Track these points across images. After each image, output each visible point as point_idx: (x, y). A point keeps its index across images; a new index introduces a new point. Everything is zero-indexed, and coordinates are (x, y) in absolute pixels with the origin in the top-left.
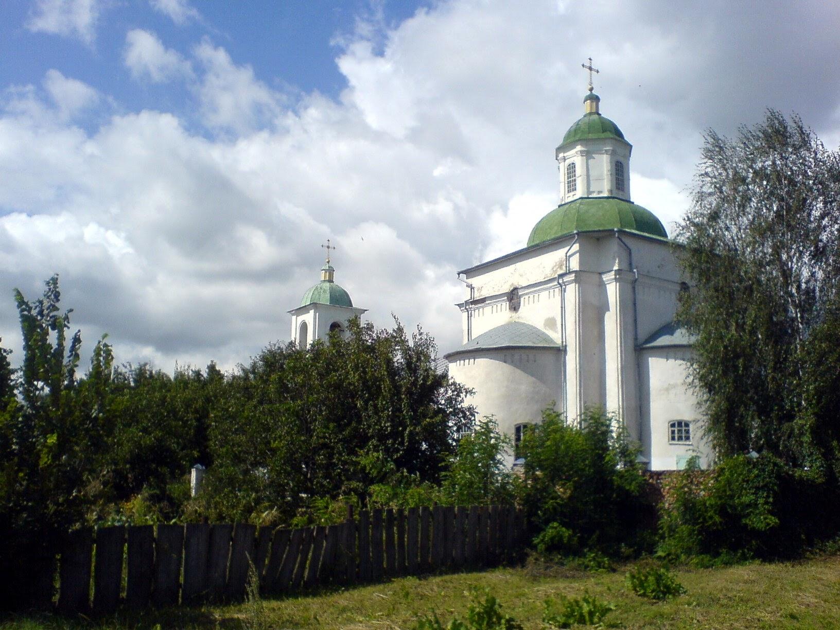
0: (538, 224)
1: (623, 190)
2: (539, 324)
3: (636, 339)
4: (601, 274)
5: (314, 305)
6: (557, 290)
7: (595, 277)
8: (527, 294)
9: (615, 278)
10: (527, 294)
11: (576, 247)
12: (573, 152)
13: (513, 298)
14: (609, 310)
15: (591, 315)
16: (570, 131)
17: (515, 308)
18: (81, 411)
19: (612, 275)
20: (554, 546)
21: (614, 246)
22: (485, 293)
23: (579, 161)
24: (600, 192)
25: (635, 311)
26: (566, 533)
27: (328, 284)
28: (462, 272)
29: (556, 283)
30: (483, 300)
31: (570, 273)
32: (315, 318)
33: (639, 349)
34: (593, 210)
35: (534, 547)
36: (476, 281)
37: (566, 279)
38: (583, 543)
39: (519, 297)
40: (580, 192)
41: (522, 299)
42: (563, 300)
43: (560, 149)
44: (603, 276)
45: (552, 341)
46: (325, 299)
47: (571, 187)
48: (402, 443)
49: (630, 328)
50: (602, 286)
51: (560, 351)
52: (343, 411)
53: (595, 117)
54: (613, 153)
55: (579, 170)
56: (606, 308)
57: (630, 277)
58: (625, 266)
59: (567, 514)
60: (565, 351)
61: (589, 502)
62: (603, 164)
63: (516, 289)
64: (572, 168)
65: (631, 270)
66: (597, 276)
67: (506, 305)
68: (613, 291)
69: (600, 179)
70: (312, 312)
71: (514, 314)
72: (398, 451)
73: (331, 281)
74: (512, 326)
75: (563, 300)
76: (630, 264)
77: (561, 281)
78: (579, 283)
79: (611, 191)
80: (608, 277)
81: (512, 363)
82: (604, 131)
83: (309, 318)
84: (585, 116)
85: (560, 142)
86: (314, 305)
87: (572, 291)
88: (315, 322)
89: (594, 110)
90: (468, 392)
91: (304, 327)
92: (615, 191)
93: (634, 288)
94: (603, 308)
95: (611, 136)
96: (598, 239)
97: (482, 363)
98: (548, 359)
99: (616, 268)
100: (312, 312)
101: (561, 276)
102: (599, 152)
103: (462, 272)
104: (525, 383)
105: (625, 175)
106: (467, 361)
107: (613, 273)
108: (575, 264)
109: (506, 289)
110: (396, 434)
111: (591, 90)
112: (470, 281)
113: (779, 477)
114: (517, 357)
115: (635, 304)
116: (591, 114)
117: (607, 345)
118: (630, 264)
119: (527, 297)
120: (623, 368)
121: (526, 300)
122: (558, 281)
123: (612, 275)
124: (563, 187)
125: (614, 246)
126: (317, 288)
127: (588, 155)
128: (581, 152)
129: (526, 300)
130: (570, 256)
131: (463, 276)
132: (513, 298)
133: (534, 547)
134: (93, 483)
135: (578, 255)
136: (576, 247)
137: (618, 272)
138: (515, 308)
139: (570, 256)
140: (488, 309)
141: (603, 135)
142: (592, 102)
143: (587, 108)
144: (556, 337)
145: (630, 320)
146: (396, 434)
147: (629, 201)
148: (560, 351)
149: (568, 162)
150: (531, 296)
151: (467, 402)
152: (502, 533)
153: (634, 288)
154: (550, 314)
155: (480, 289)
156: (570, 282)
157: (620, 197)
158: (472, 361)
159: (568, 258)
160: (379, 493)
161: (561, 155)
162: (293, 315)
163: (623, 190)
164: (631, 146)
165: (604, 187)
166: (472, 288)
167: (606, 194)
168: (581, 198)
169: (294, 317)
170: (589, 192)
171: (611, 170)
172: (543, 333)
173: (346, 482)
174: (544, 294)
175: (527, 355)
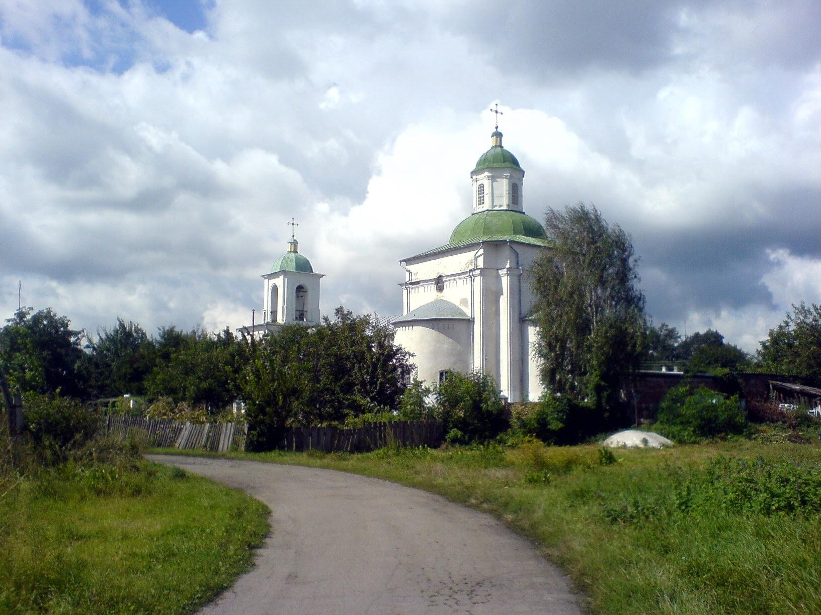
0: (458, 226)
2: (457, 303)
5: (284, 272)
7: (494, 272)
11: (481, 251)
12: (482, 176)
13: (439, 283)
15: (491, 297)
17: (440, 289)
19: (505, 271)
20: (455, 441)
21: (506, 251)
22: (420, 277)
23: (487, 183)
24: (501, 206)
26: (460, 433)
27: (293, 255)
28: (404, 261)
30: (418, 283)
34: (495, 221)
35: (445, 440)
36: (412, 268)
38: (470, 439)
39: (443, 282)
40: (487, 206)
42: (472, 286)
45: (465, 314)
46: (292, 267)
47: (481, 201)
48: (375, 388)
49: (517, 307)
50: (498, 278)
51: (470, 322)
52: (340, 369)
53: (499, 149)
55: (487, 190)
57: (516, 272)
58: (514, 265)
59: (462, 424)
61: (474, 417)
62: (503, 185)
63: (441, 276)
64: (481, 188)
65: (518, 268)
67: (434, 287)
68: (505, 281)
69: (501, 196)
70: (282, 277)
72: (372, 392)
73: (295, 252)
74: (439, 304)
75: (472, 286)
76: (518, 263)
79: (508, 206)
80: (502, 272)
81: (438, 330)
83: (279, 281)
85: (473, 167)
86: (284, 272)
87: (478, 281)
91: (275, 289)
94: (499, 293)
97: (418, 329)
98: (462, 327)
99: (508, 266)
100: (282, 277)
101: (471, 271)
104: (446, 343)
108: (480, 263)
109: (435, 276)
110: (372, 383)
111: (497, 128)
112: (408, 267)
113: (570, 405)
116: (496, 146)
118: (518, 263)
120: (511, 334)
122: (469, 274)
123: (505, 271)
124: (475, 201)
125: (506, 251)
127: (493, 179)
132: (439, 283)
133: (445, 440)
136: (481, 251)
137: (509, 269)
138: (440, 289)
140: (421, 289)
145: (516, 301)
146: (372, 383)
148: (470, 322)
149: (479, 183)
152: (430, 432)
154: (464, 296)
156: (477, 275)
159: (476, 258)
160: (369, 416)
161: (474, 177)
165: (504, 202)
166: (410, 273)
167: (505, 208)
170: (493, 206)
172: (459, 309)
174: (460, 282)
175: (448, 325)
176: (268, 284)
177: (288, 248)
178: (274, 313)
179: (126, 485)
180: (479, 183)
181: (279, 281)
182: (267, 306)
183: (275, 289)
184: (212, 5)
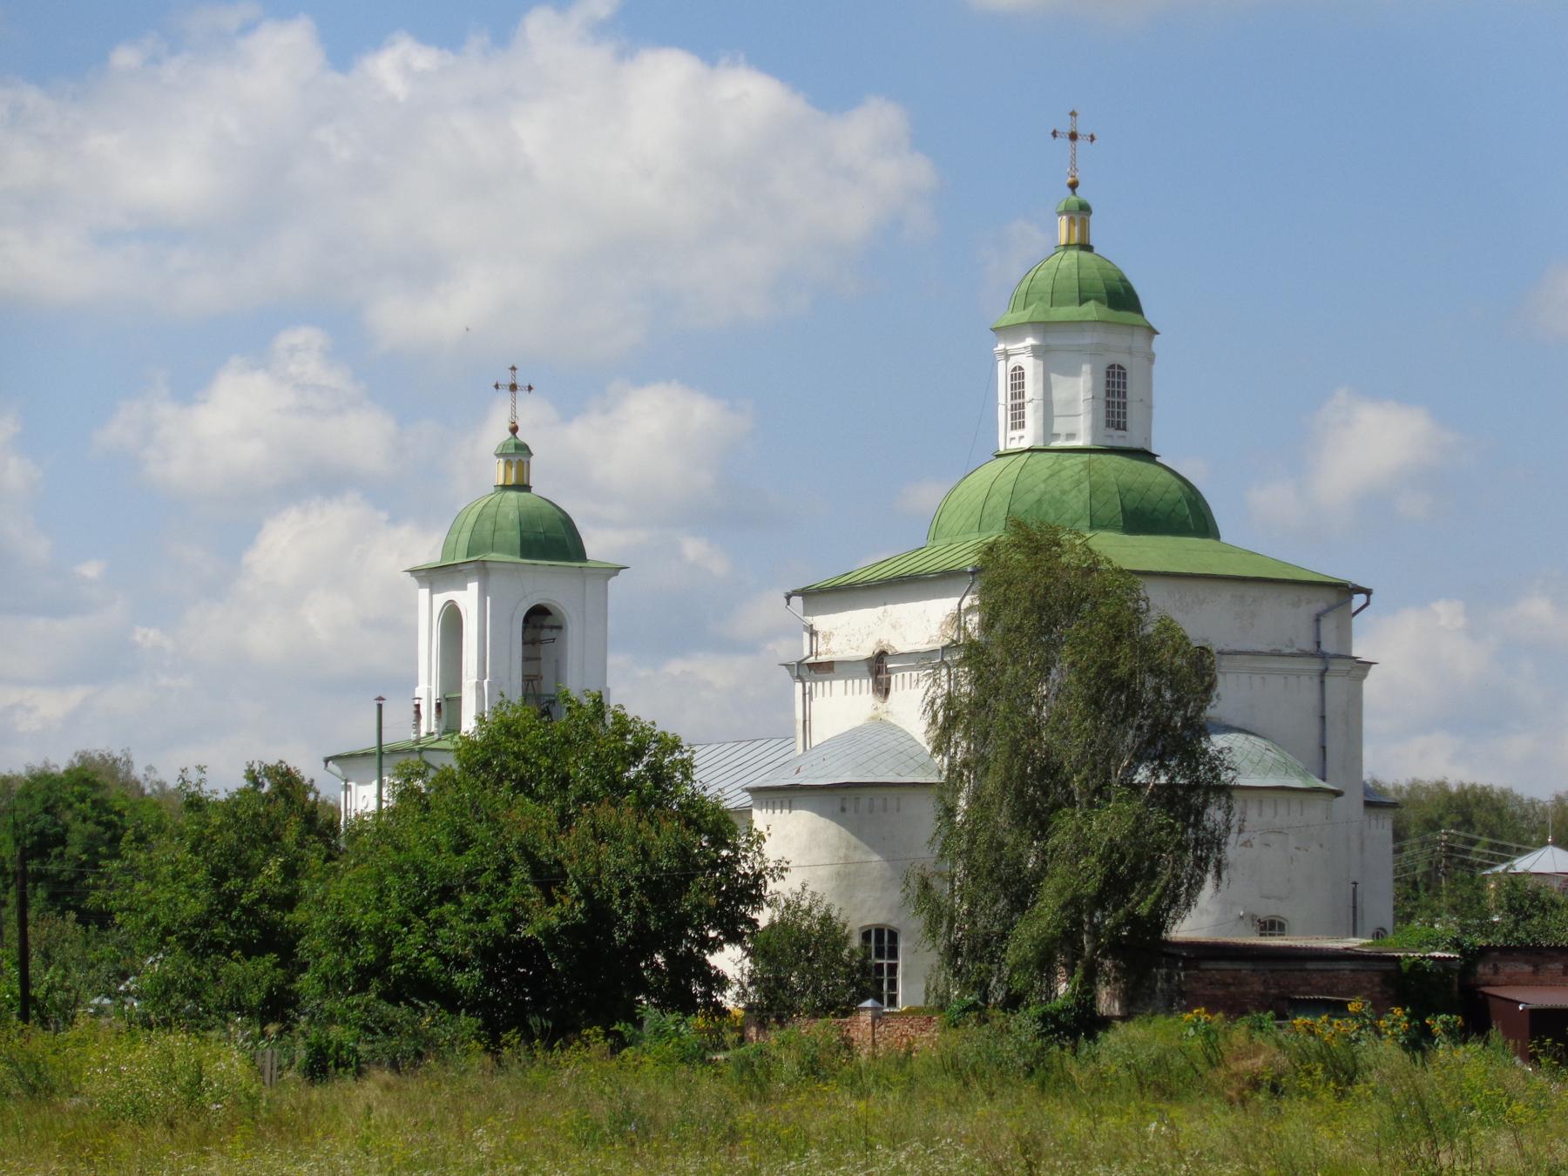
17: (882, 689)
18: (957, 1153)
23: (1029, 364)
24: (1071, 436)
28: (795, 593)
36: (821, 622)
55: (1032, 389)
67: (867, 684)
73: (523, 487)
82: (1083, 301)
83: (468, 598)
89: (1075, 239)
91: (452, 620)
95: (1094, 316)
100: (473, 587)
109: (867, 651)
114: (864, 802)
128: (1034, 348)
131: (797, 601)
134: (700, 1020)
138: (882, 689)
140: (838, 685)
147: (1146, 455)
149: (1013, 362)
155: (828, 637)
165: (1081, 430)
166: (813, 633)
170: (1048, 433)
171: (1094, 388)
173: (1446, 916)
176: (428, 605)
177: (498, 472)
178: (448, 706)
179: (432, 1123)
180: (1013, 362)
181: (468, 598)
182: (427, 689)
183: (452, 620)
184: (7, 782)
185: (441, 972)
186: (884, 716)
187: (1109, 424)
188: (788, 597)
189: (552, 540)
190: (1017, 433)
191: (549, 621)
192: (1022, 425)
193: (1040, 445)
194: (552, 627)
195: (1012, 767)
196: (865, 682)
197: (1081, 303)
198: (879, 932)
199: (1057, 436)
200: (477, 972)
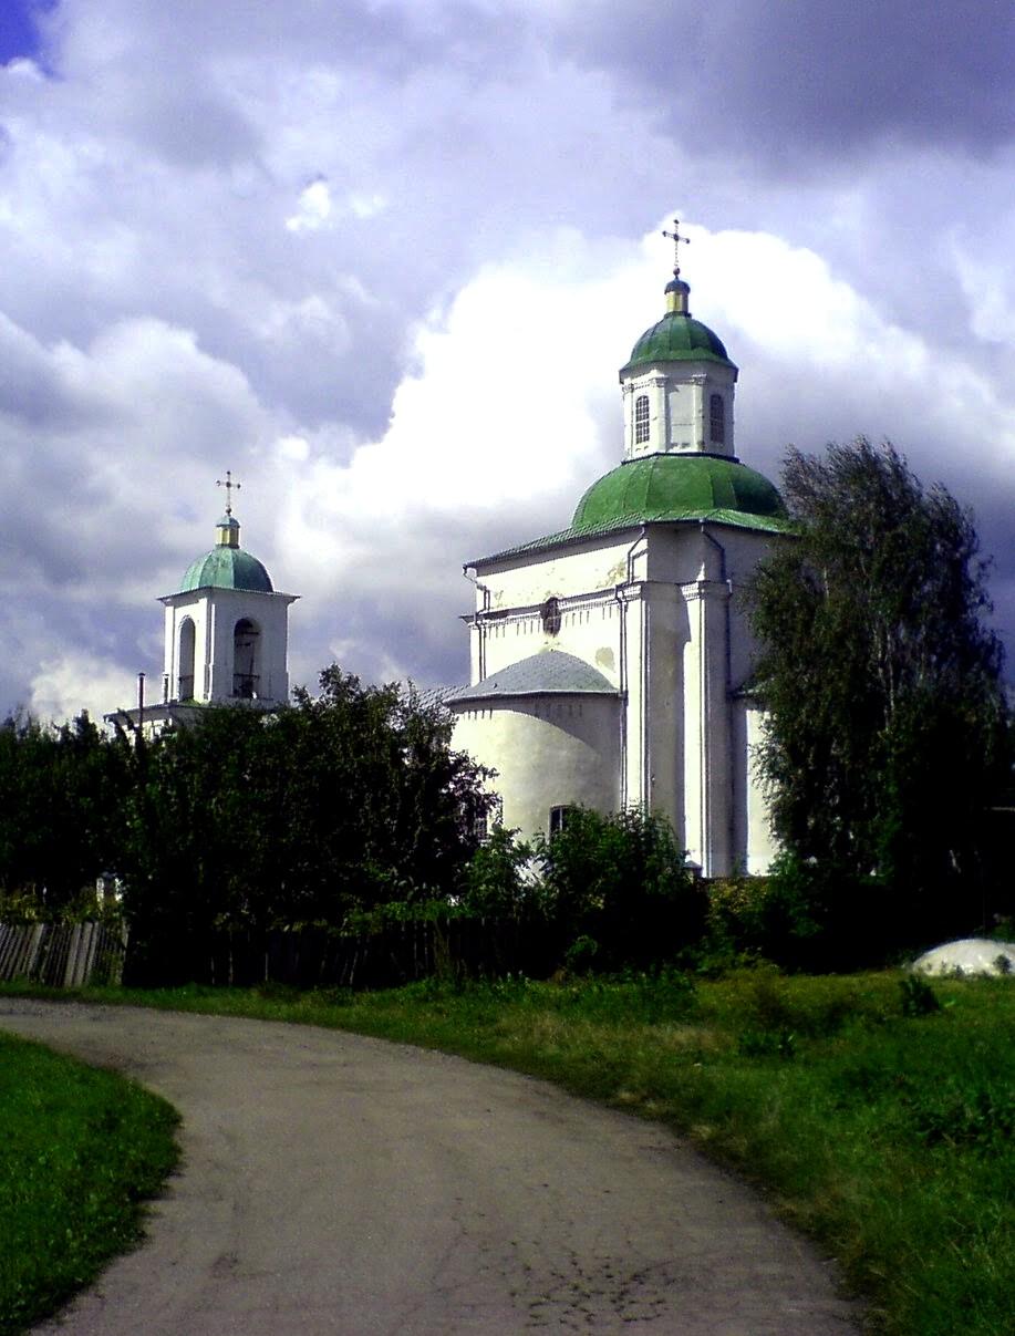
1: (722, 441)
2: (589, 658)
3: (728, 682)
4: (679, 585)
5: (207, 591)
6: (615, 607)
7: (670, 591)
8: (570, 610)
9: (700, 593)
10: (570, 610)
11: (643, 545)
12: (644, 378)
13: (550, 614)
14: (690, 641)
15: (664, 645)
16: (634, 352)
17: (552, 628)
21: (699, 545)
22: (508, 602)
23: (655, 395)
24: (685, 445)
25: (728, 640)
28: (472, 565)
29: (612, 597)
30: (504, 614)
31: (634, 584)
32: (209, 614)
33: (729, 700)
36: (490, 581)
37: (628, 592)
39: (558, 613)
40: (655, 444)
41: (563, 616)
42: (623, 622)
43: (625, 372)
44: (683, 589)
45: (606, 684)
46: (226, 579)
47: (642, 434)
50: (681, 603)
51: (619, 700)
53: (681, 320)
54: (707, 383)
55: (656, 409)
56: (684, 636)
58: (715, 573)
60: (626, 699)
61: (621, 899)
62: (691, 399)
63: (554, 600)
64: (643, 405)
65: (723, 581)
66: (675, 587)
67: (538, 623)
68: (695, 611)
69: (686, 424)
70: (203, 602)
71: (550, 638)
73: (234, 545)
74: (550, 661)
75: (623, 622)
76: (723, 572)
77: (620, 595)
78: (647, 600)
79: (702, 444)
80: (689, 591)
81: (549, 718)
83: (199, 611)
84: (667, 316)
85: (625, 359)
86: (207, 591)
87: (636, 609)
88: (209, 620)
90: (492, 774)
91: (189, 628)
92: (709, 443)
93: (727, 607)
95: (705, 356)
96: (676, 531)
97: (503, 718)
98: (601, 711)
99: (701, 577)
100: (203, 602)
101: (620, 587)
102: (686, 381)
103: (472, 565)
104: (566, 748)
105: (726, 415)
106: (480, 713)
107: (697, 584)
108: (641, 570)
109: (540, 599)
112: (482, 580)
115: (728, 631)
116: (675, 314)
117: (685, 691)
119: (570, 614)
121: (570, 619)
122: (616, 594)
125: (699, 545)
126: (210, 559)
127: (668, 385)
129: (570, 619)
130: (634, 558)
132: (550, 614)
135: (646, 555)
136: (643, 545)
138: (552, 628)
139: (634, 558)
140: (511, 627)
141: (692, 354)
142: (678, 294)
143: (664, 305)
144: (613, 678)
145: (720, 658)
148: (619, 700)
149: (638, 393)
150: (577, 612)
151: (488, 787)
153: (727, 607)
154: (605, 643)
156: (634, 598)
157: (718, 452)
158: (487, 712)
159: (631, 559)
161: (627, 381)
162: (167, 605)
163: (722, 441)
164: (736, 370)
165: (692, 437)
166: (486, 592)
167: (694, 449)
168: (656, 454)
169: (169, 610)
170: (669, 445)
174: (596, 612)
175: (569, 707)
176: (174, 617)
177: (218, 536)
178: (187, 680)
181: (199, 611)
182: (172, 666)
183: (189, 628)
185: (136, 1231)
186: (555, 648)
187: (712, 439)
188: (465, 569)
189: (252, 578)
190: (643, 444)
191: (250, 630)
192: (647, 439)
193: (664, 451)
194: (252, 633)
195: (999, 660)
196: (535, 621)
197: (693, 348)
198: (566, 811)
199: (676, 445)
200: (217, 923)
